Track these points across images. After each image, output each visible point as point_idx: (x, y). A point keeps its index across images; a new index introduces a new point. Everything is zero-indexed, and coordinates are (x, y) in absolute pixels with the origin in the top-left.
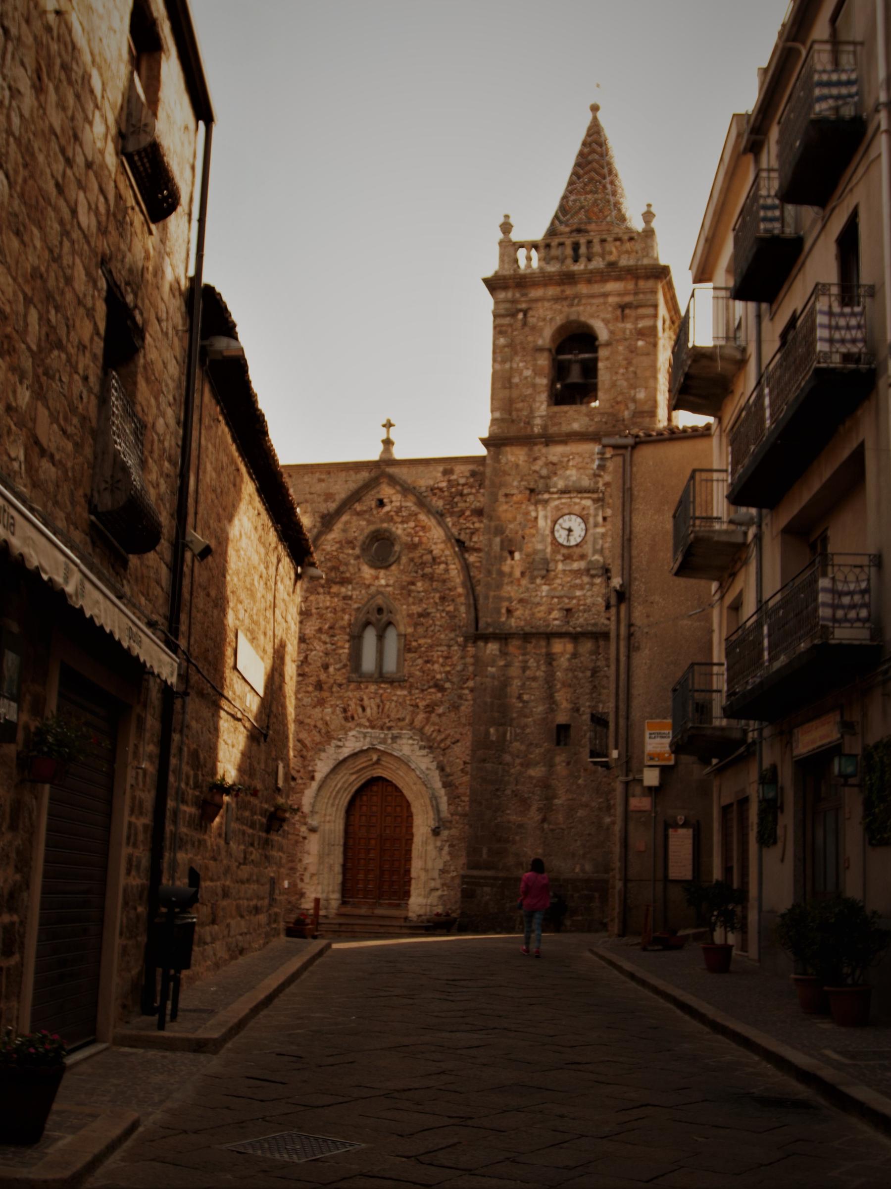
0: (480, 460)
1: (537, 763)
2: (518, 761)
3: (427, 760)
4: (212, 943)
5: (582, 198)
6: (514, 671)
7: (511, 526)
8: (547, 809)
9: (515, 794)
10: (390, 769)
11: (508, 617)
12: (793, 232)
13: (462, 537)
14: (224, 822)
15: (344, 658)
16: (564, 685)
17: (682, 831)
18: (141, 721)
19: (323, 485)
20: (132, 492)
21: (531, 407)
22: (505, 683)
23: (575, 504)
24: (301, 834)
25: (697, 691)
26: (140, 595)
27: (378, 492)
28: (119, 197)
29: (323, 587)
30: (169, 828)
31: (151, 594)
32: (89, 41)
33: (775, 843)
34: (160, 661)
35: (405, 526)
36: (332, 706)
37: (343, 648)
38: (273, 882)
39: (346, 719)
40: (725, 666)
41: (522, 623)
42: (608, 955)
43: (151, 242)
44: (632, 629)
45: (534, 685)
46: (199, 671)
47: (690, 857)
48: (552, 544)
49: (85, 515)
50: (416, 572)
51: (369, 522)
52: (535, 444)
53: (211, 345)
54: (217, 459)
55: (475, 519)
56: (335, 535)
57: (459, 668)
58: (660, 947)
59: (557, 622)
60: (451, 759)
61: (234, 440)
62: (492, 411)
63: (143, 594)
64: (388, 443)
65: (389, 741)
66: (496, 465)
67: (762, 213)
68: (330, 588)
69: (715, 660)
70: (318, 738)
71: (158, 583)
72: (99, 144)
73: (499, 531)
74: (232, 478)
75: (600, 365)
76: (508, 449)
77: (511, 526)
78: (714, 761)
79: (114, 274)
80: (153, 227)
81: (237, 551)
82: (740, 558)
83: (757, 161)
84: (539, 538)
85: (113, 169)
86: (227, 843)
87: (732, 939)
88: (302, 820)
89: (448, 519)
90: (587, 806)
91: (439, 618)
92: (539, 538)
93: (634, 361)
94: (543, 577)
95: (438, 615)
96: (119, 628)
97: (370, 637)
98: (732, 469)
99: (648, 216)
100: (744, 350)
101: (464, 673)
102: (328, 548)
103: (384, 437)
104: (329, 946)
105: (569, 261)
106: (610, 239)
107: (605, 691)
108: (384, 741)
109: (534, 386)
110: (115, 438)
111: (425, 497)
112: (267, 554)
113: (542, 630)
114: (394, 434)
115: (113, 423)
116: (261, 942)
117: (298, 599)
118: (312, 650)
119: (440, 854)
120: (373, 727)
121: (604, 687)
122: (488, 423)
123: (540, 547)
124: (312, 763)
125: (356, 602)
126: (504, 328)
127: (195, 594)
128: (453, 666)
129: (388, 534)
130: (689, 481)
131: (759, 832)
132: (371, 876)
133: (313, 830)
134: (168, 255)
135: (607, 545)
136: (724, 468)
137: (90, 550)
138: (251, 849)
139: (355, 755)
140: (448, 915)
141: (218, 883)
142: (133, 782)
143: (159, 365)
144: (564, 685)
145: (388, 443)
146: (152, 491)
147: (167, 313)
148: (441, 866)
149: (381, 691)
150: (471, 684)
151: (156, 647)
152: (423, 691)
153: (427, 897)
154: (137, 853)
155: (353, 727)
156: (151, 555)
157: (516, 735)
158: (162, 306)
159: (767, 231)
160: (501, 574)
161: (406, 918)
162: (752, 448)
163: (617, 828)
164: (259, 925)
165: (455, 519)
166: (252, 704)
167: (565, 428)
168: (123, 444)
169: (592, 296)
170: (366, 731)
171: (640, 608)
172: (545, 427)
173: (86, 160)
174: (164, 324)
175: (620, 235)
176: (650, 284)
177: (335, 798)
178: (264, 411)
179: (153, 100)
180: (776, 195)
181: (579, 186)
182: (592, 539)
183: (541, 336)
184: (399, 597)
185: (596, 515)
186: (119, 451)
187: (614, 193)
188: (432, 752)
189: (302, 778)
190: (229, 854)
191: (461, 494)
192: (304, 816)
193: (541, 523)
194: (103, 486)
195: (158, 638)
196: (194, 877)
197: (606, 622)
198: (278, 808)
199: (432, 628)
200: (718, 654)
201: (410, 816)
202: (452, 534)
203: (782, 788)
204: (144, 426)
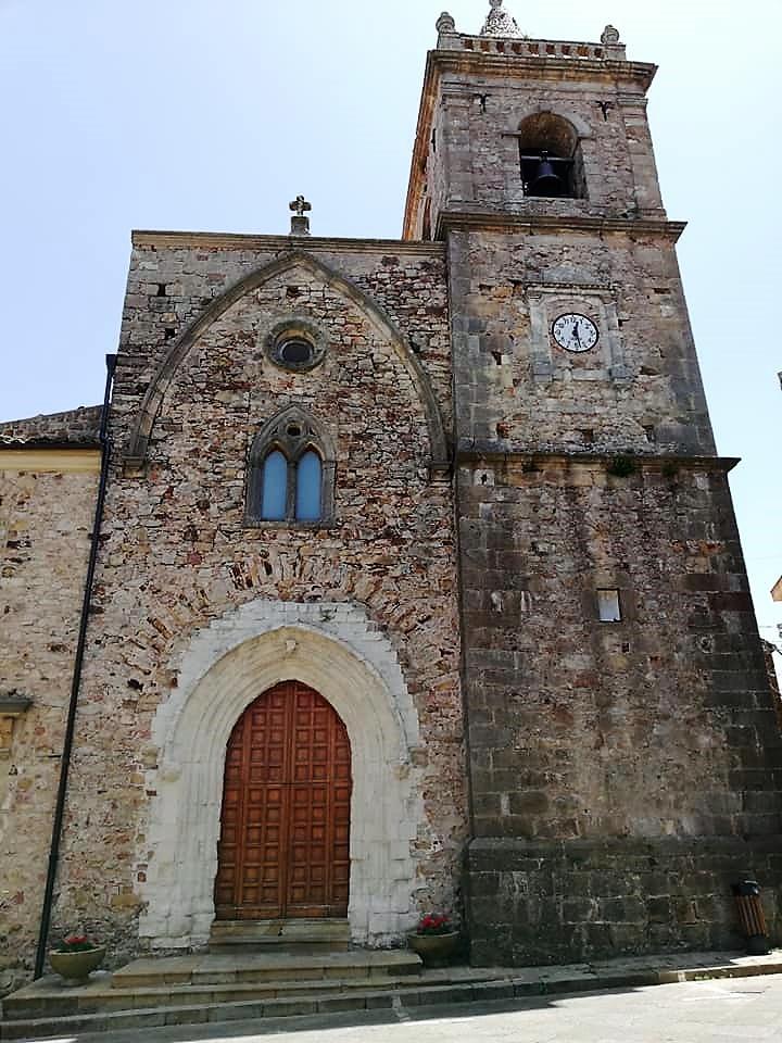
1: (574, 648)
6: (520, 509)
29: (202, 392)
37: (231, 478)
39: (238, 584)
45: (553, 529)
50: (350, 381)
51: (276, 313)
55: (433, 320)
57: (423, 510)
59: (571, 446)
88: (149, 760)
90: (666, 717)
102: (212, 342)
149: (298, 543)
152: (367, 542)
160: (484, 381)
177: (212, 720)
188: (386, 637)
193: (535, 320)
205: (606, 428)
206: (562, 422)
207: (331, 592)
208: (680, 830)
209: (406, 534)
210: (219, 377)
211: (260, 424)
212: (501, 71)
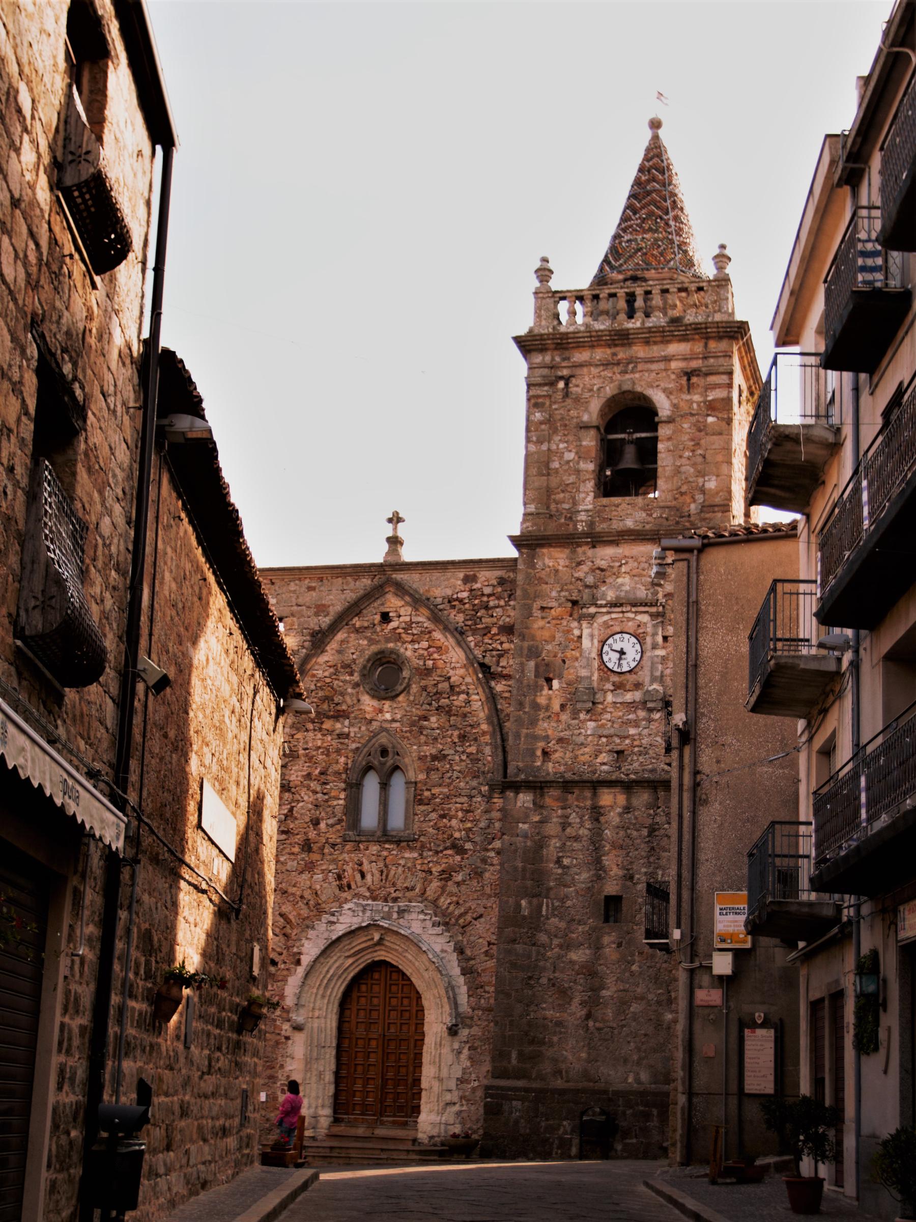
0: (509, 564)
2: (556, 942)
3: (442, 940)
4: (166, 1175)
5: (639, 237)
6: (552, 828)
7: (549, 647)
8: (593, 1003)
9: (552, 983)
10: (396, 950)
11: (544, 761)
12: (898, 285)
13: (487, 661)
14: (183, 1021)
15: (339, 811)
16: (614, 846)
17: (760, 1032)
18: (78, 896)
19: (314, 594)
20: (69, 612)
21: (574, 498)
22: (541, 844)
23: (629, 619)
24: (283, 1033)
25: (779, 856)
26: (79, 738)
27: (383, 604)
28: (54, 242)
29: (313, 722)
30: (112, 1029)
31: (92, 738)
32: (15, 48)
33: (876, 1049)
34: (102, 821)
35: (416, 646)
36: (323, 871)
38: (246, 1096)
39: (341, 888)
40: (813, 826)
41: (562, 768)
42: (667, 1189)
43: (96, 297)
44: (699, 777)
46: (153, 832)
47: (772, 1065)
48: (599, 669)
49: (10, 640)
50: (430, 704)
51: (371, 641)
52: (579, 545)
53: (171, 426)
54: (178, 566)
55: (504, 639)
56: (328, 656)
57: (482, 824)
58: (734, 1180)
59: (605, 768)
60: (472, 938)
61: (200, 543)
62: (525, 504)
63: (82, 738)
64: (394, 542)
65: (395, 916)
66: (530, 571)
67: (860, 262)
68: (322, 723)
69: (802, 818)
70: (305, 912)
71: (102, 722)
72: (28, 177)
73: (534, 653)
74: (197, 589)
75: (661, 446)
76: (545, 551)
77: (549, 647)
78: (801, 944)
79: (48, 339)
80: (97, 279)
81: (203, 680)
82: (832, 691)
83: (855, 195)
84: (583, 662)
85: (46, 208)
86: (187, 1048)
87: (824, 1171)
88: (285, 1015)
89: (470, 639)
90: (642, 998)
91: (459, 762)
92: (583, 662)
93: (703, 442)
94: (588, 712)
95: (457, 758)
96: (51, 780)
97: (371, 785)
98: (822, 581)
99: (722, 259)
100: (838, 431)
101: (488, 831)
102: (320, 673)
103: (390, 534)
104: (315, 1177)
105: (622, 316)
106: (673, 289)
107: (666, 854)
108: (387, 916)
109: (578, 472)
110: (48, 543)
111: (441, 610)
112: (241, 683)
113: (586, 777)
114: (402, 531)
115: (46, 524)
116: (230, 1172)
117: (279, 738)
118: (298, 801)
119: (458, 1058)
120: (374, 899)
121: (665, 850)
122: (520, 518)
123: (584, 673)
124: (298, 944)
125: (354, 742)
126: (540, 400)
127: (148, 735)
128: (476, 821)
129: (394, 656)
130: (769, 594)
131: (856, 1035)
132: (370, 1087)
133: (298, 1028)
134: (117, 312)
135: (668, 671)
136: (814, 578)
137: (15, 685)
138: (218, 1054)
139: (351, 934)
140: (467, 1136)
141: (175, 1098)
142: (68, 973)
143: (105, 451)
144: (614, 846)
145: (394, 542)
146: (95, 609)
147: (115, 386)
148: (459, 1074)
149: (385, 853)
150: (497, 844)
151: (97, 804)
152: (437, 852)
153: (441, 1113)
154: (71, 1062)
155: (349, 898)
156: (94, 688)
157: (554, 909)
158: (108, 377)
159: (865, 282)
160: (536, 706)
161: (415, 1141)
162: (847, 554)
163: (680, 1027)
164: (228, 1152)
165: (479, 638)
166: (221, 871)
167: (616, 525)
168: (57, 551)
169: (651, 361)
170: (365, 902)
171: (708, 751)
172: (591, 524)
173: (12, 197)
174: (111, 400)
175: (686, 285)
176: (723, 345)
178: (237, 506)
179: (98, 119)
180: (877, 240)
181: (635, 222)
182: (649, 664)
183: (586, 410)
184: (408, 734)
185: (654, 634)
186: (53, 559)
187: (679, 232)
189: (285, 963)
190: (190, 1061)
191: (487, 608)
192: (286, 1011)
193: (586, 643)
194: (32, 603)
195: (101, 791)
196: (144, 1092)
197: (666, 767)
198: (253, 1002)
199: (449, 775)
200: (805, 811)
201: (421, 1010)
202: (475, 657)
203: (885, 981)
204: (85, 527)
205: (636, 749)
206: (597, 745)
207: (407, 894)
208: (638, 1080)
209: (468, 846)
210: (325, 706)
211: (357, 748)
212: (586, 344)
